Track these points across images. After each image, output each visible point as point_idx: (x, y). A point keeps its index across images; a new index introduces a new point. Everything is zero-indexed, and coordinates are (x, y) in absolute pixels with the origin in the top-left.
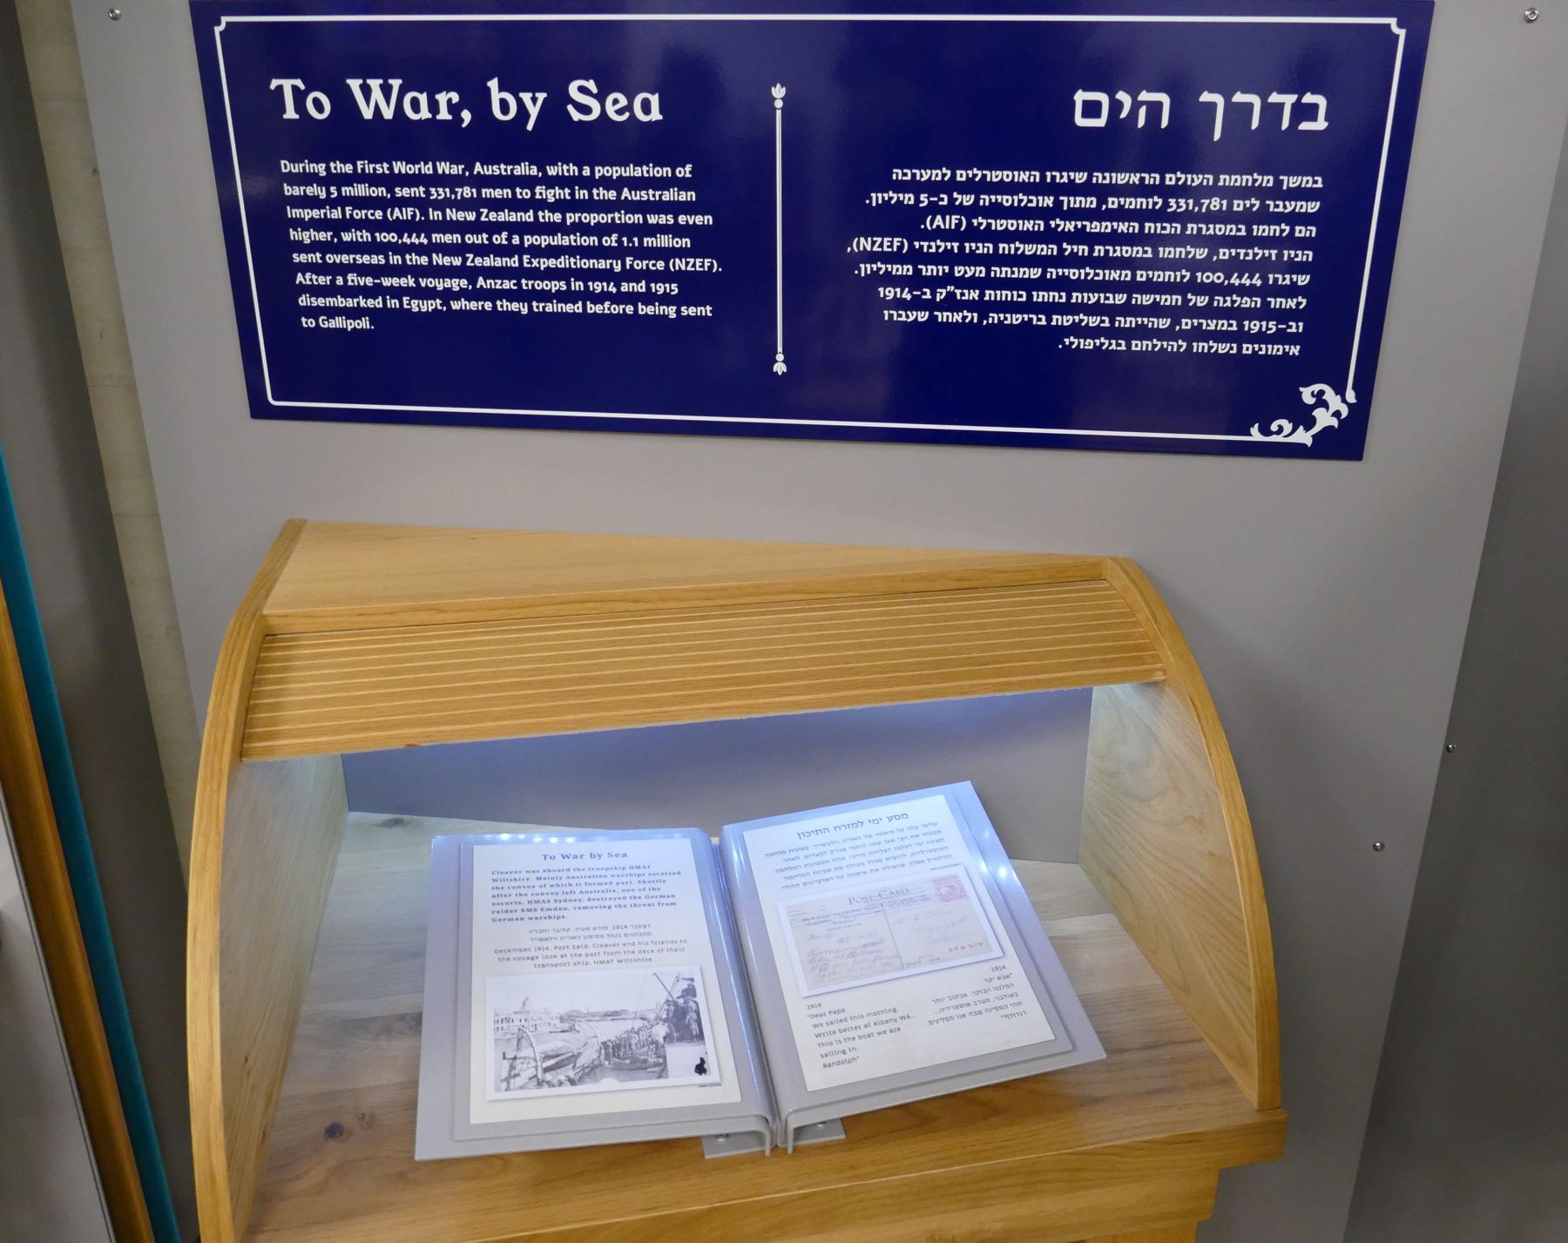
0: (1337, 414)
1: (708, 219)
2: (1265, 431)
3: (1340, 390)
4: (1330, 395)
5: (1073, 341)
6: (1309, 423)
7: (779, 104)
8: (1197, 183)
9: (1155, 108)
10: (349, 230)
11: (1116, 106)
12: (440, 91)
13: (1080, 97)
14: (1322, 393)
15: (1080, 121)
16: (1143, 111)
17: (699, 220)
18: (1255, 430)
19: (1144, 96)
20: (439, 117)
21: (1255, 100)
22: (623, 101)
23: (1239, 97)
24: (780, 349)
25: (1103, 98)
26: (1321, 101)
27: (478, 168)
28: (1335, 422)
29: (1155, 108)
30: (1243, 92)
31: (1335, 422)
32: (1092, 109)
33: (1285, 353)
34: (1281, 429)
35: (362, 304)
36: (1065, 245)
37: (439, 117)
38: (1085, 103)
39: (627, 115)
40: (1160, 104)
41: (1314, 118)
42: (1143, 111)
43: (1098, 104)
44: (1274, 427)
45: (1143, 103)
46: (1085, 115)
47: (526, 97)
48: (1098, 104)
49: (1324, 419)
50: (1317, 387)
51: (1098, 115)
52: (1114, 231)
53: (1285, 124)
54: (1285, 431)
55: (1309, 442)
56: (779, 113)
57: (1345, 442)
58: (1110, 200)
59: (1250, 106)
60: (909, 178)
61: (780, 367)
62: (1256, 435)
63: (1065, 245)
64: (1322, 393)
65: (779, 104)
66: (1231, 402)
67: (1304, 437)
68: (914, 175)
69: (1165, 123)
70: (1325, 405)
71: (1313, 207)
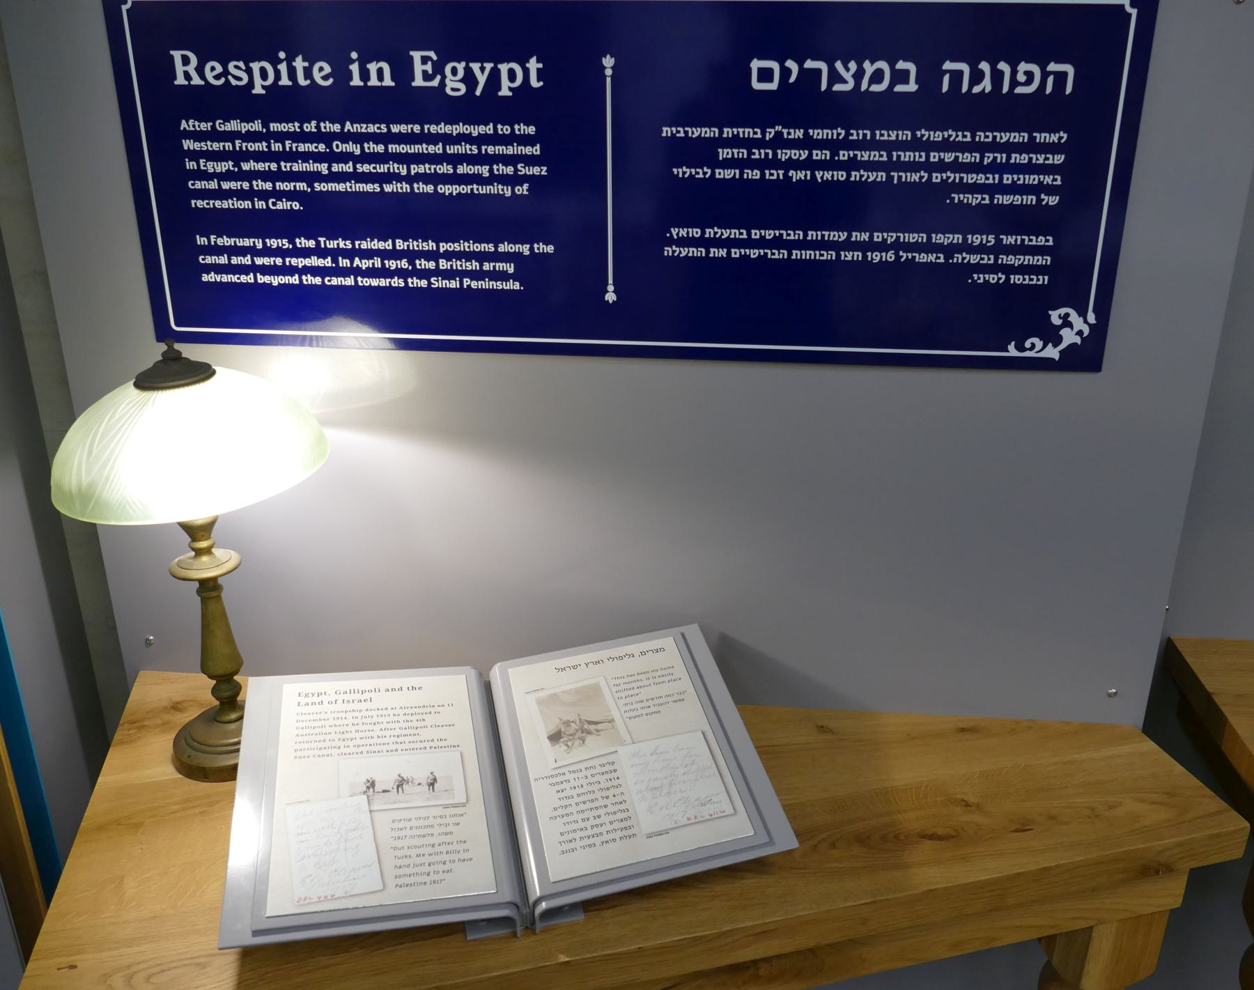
0: (1080, 333)
1: (544, 171)
2: (1020, 348)
3: (1083, 313)
4: (1074, 317)
5: (980, 278)
6: (1057, 340)
7: (609, 72)
8: (1005, 139)
9: (1061, 77)
10: (390, 182)
11: (785, 72)
12: (370, 62)
13: (756, 64)
14: (1067, 315)
15: (757, 85)
16: (1050, 80)
17: (536, 170)
18: (1011, 347)
19: (1052, 67)
20: (280, 83)
21: (822, 66)
22: (219, 69)
23: (809, 64)
24: (610, 281)
25: (775, 66)
26: (911, 67)
27: (348, 126)
28: (1078, 340)
29: (1061, 77)
30: (905, 60)
31: (1078, 340)
32: (765, 75)
33: (987, 282)
34: (1033, 346)
35: (342, 245)
36: (1043, 196)
37: (280, 83)
38: (760, 70)
39: (223, 80)
40: (1065, 74)
41: (907, 82)
42: (1050, 80)
43: (771, 71)
44: (1028, 344)
45: (1051, 73)
46: (760, 80)
47: (475, 67)
48: (771, 71)
49: (1069, 337)
50: (1063, 311)
51: (771, 80)
52: (1040, 183)
53: (824, 87)
54: (1037, 348)
55: (1056, 356)
56: (609, 80)
57: (1086, 357)
58: (841, 153)
59: (819, 71)
60: (990, 140)
61: (611, 297)
62: (1012, 351)
63: (1043, 196)
64: (1067, 315)
65: (609, 72)
66: (969, 322)
67: (1052, 353)
68: (995, 137)
69: (1069, 90)
70: (1070, 325)
71: (1059, 159)
